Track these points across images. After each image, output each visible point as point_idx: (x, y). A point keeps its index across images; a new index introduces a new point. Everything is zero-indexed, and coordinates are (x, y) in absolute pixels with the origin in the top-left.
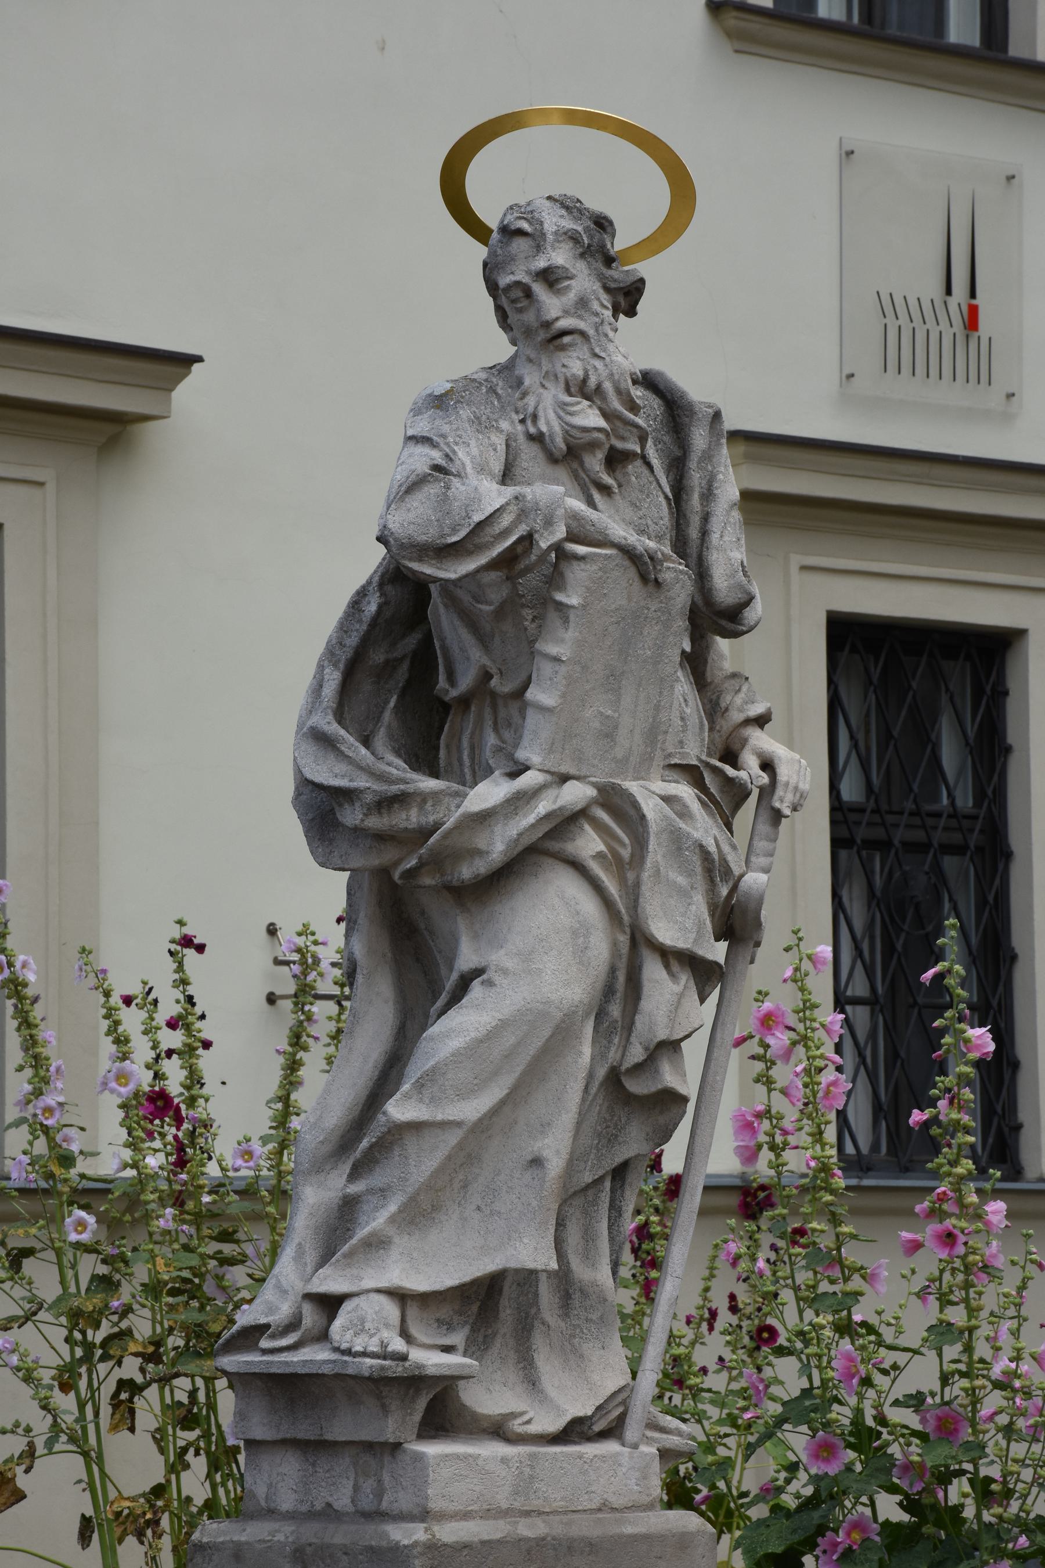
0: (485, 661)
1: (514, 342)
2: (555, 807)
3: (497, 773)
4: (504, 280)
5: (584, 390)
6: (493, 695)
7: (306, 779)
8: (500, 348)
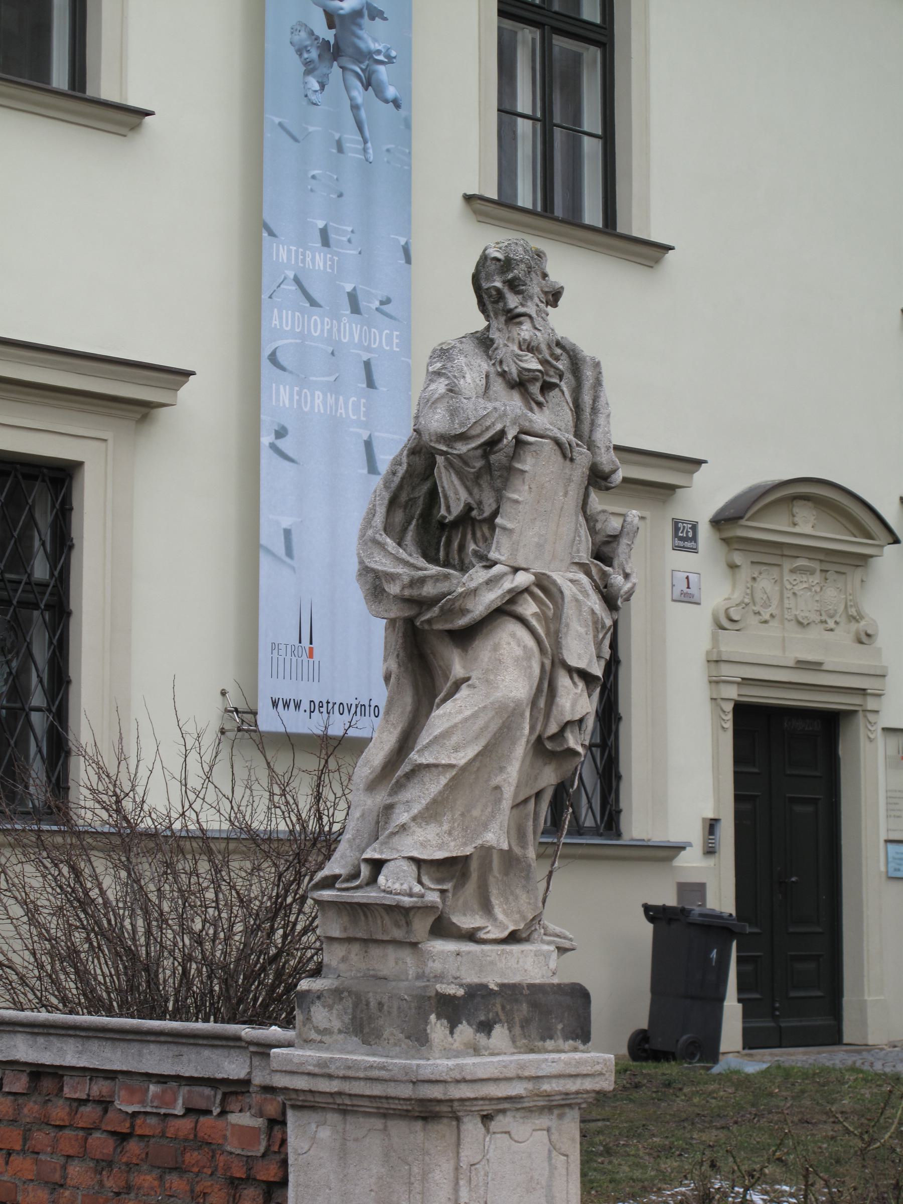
0: (470, 500)
1: (487, 318)
2: (513, 586)
3: (477, 566)
4: (485, 285)
5: (531, 348)
6: (473, 520)
7: (367, 567)
8: (479, 323)
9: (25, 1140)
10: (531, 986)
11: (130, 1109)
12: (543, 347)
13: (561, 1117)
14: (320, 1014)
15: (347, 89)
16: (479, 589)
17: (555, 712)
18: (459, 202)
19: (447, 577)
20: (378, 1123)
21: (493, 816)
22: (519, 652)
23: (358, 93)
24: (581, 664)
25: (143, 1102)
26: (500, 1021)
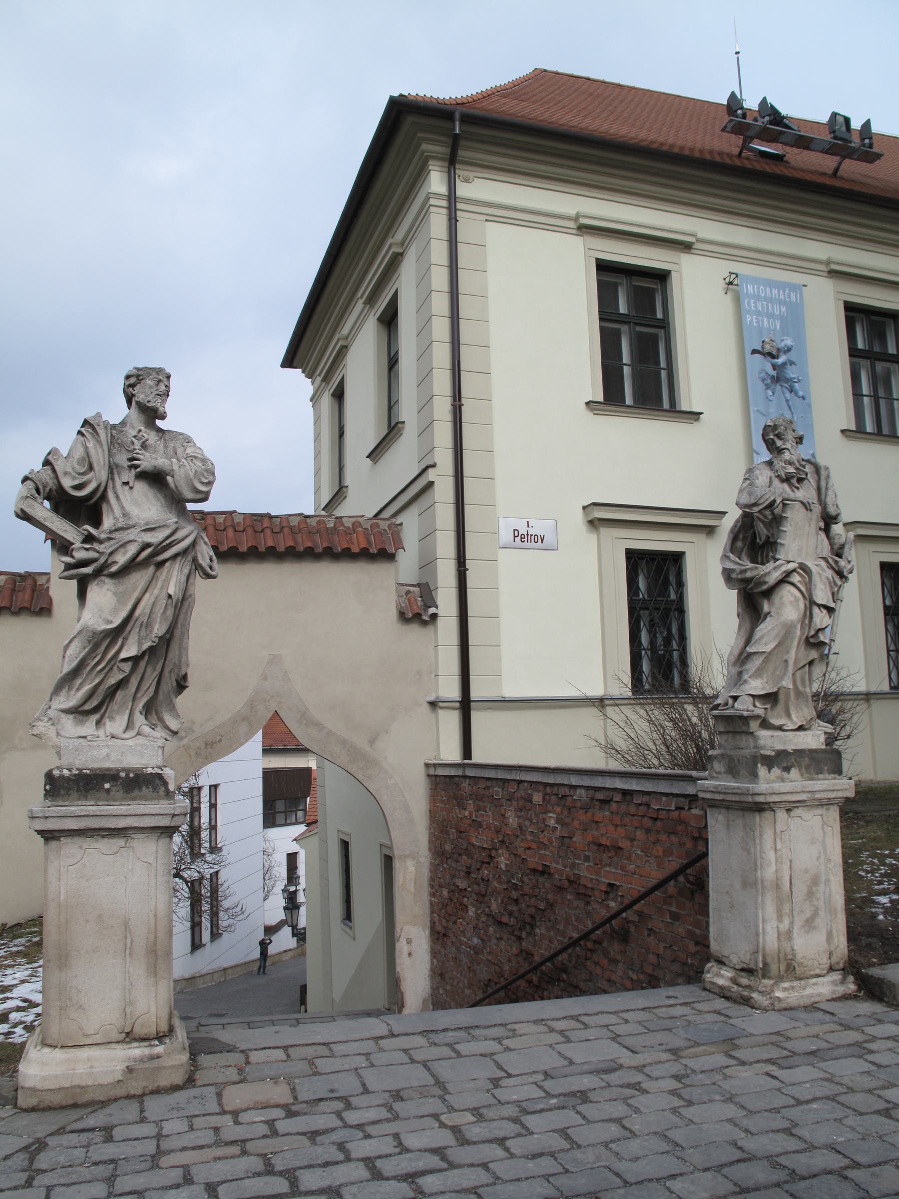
5: (790, 463)
9: (622, 820)
10: (810, 750)
11: (656, 808)
12: (796, 462)
13: (828, 809)
14: (717, 766)
15: (784, 394)
16: (771, 572)
17: (813, 625)
18: (839, 433)
19: (756, 568)
20: (740, 813)
21: (784, 674)
22: (792, 599)
23: (788, 395)
24: (824, 603)
25: (660, 805)
26: (794, 766)
